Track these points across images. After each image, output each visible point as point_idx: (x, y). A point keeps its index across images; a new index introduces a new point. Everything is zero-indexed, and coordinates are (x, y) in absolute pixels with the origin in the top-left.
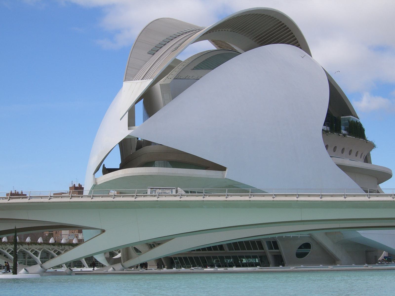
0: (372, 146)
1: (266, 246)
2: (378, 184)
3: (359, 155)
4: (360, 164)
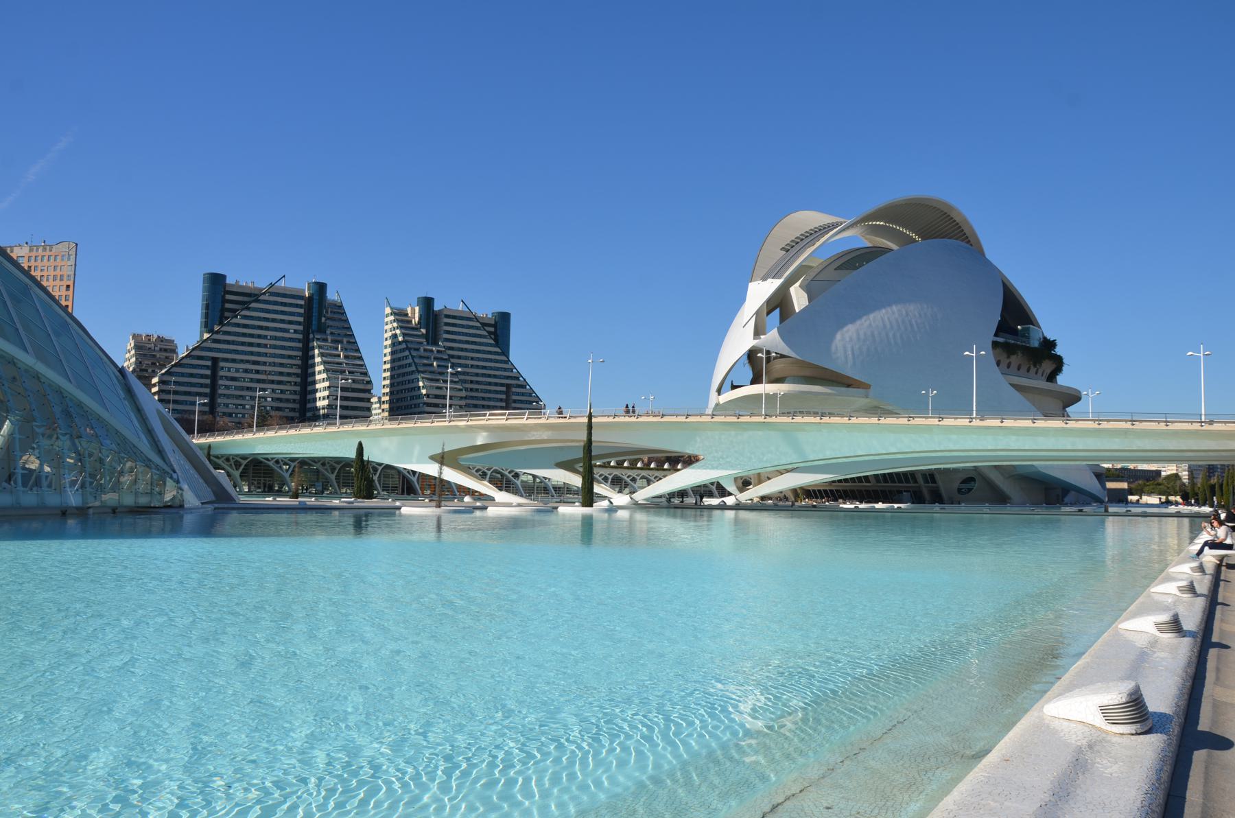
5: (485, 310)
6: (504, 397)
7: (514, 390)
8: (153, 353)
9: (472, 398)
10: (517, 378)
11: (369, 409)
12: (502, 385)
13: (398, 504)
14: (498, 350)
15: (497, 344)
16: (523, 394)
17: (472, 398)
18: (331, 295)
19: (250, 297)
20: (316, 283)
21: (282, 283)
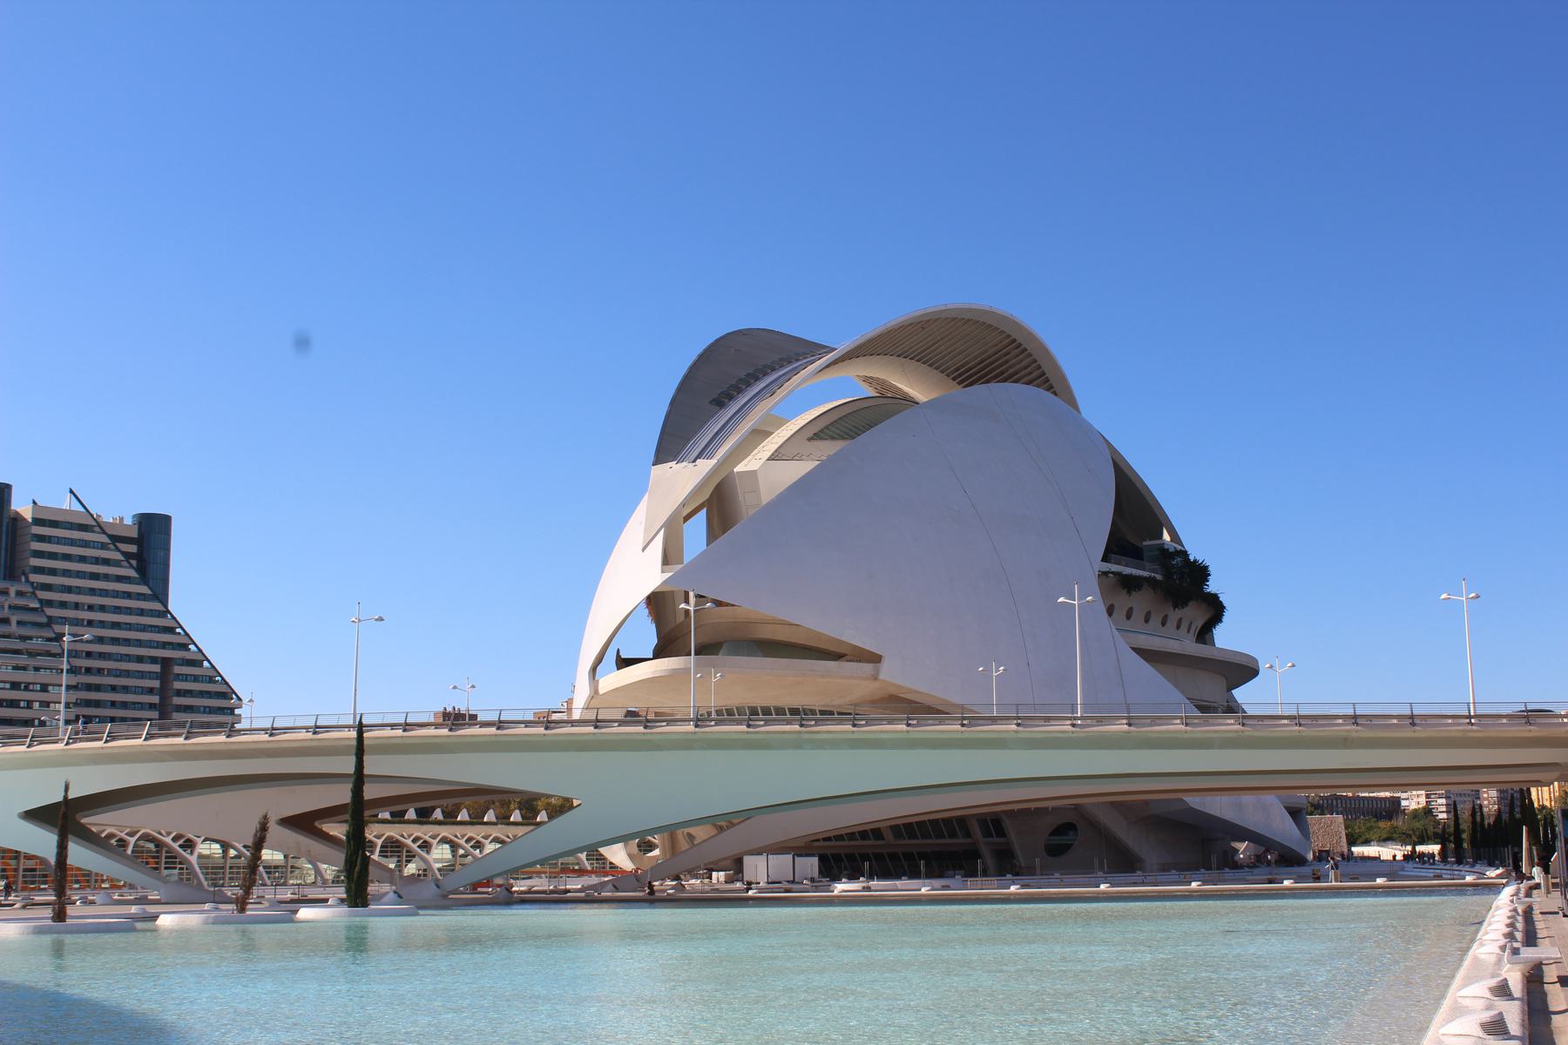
2: (1230, 689)
3: (1184, 626)
5: (117, 508)
6: (156, 684)
7: (177, 669)
9: (89, 687)
10: (184, 647)
12: (154, 660)
14: (144, 589)
15: (144, 578)
16: (196, 679)
17: (89, 687)
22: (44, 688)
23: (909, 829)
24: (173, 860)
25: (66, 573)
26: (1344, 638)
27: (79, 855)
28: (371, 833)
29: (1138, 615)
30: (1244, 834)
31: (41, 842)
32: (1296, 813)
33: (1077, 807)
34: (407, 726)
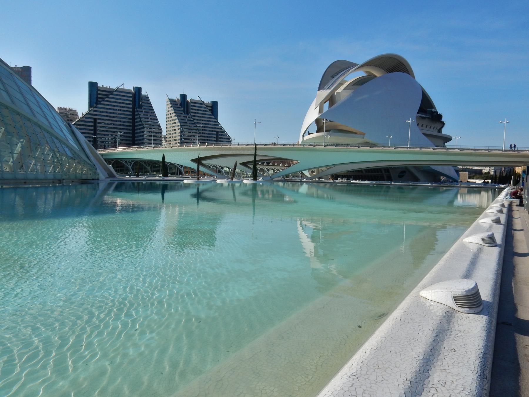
0: (443, 124)
1: (383, 172)
4: (435, 133)
5: (207, 99)
6: (216, 136)
7: (220, 133)
8: (67, 115)
9: (203, 136)
10: (221, 129)
11: (161, 140)
12: (215, 131)
13: (181, 179)
14: (213, 117)
15: (213, 114)
16: (223, 135)
17: (203, 136)
18: (143, 93)
19: (109, 92)
20: (136, 87)
21: (122, 87)
22: (194, 136)
23: (368, 170)
24: (219, 171)
25: (198, 113)
26: (467, 133)
27: (202, 169)
28: (258, 167)
29: (425, 126)
30: (443, 175)
31: (194, 166)
32: (457, 171)
33: (406, 168)
34: (265, 145)
